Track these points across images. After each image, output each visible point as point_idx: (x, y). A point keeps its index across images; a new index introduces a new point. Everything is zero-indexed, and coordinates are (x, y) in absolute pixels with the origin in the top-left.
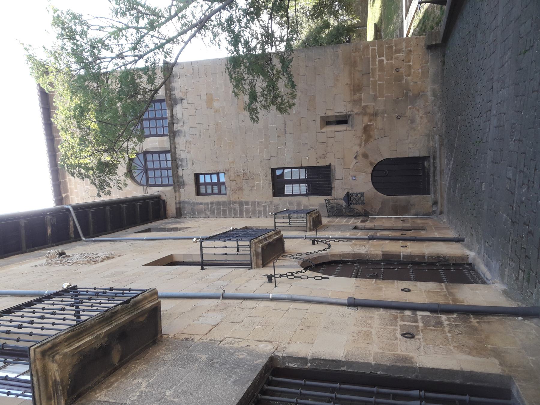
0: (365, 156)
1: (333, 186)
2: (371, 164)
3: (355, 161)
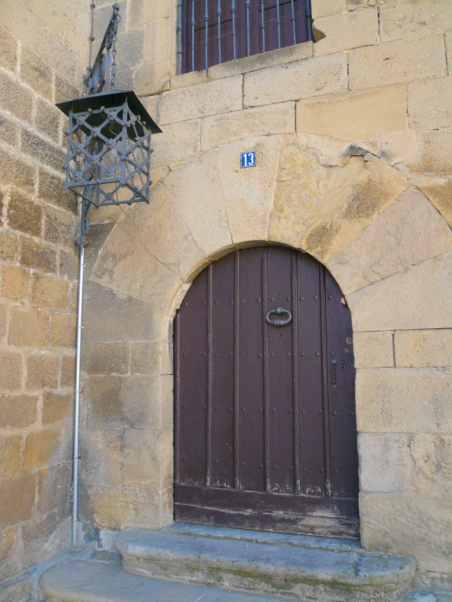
0: (364, 202)
1: (216, 71)
2: (322, 234)
3: (333, 152)
